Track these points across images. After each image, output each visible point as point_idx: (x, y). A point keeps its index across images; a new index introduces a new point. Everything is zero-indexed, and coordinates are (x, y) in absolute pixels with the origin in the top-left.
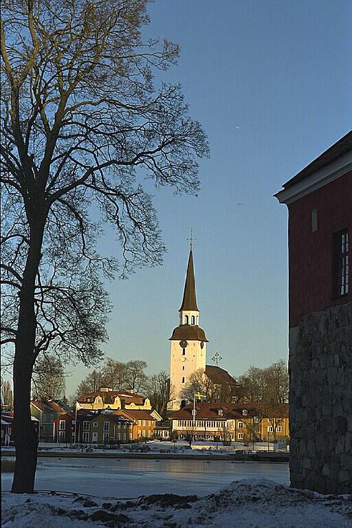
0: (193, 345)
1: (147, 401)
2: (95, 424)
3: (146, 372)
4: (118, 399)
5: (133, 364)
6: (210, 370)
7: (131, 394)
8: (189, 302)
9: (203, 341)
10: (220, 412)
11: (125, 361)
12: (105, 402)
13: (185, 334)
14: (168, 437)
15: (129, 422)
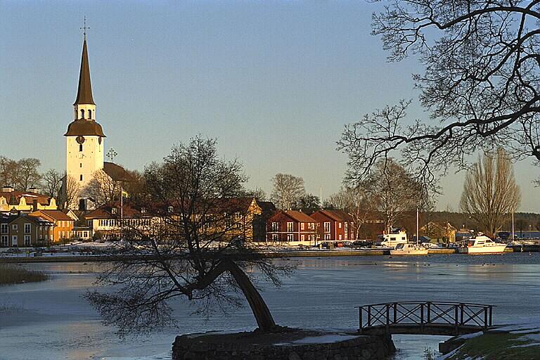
0: (91, 140)
1: (53, 201)
2: (15, 227)
3: (40, 170)
4: (23, 199)
5: (24, 162)
6: (109, 168)
7: (35, 194)
8: (84, 95)
9: (101, 136)
12: (10, 203)
13: (82, 129)
14: (88, 238)
15: (50, 223)
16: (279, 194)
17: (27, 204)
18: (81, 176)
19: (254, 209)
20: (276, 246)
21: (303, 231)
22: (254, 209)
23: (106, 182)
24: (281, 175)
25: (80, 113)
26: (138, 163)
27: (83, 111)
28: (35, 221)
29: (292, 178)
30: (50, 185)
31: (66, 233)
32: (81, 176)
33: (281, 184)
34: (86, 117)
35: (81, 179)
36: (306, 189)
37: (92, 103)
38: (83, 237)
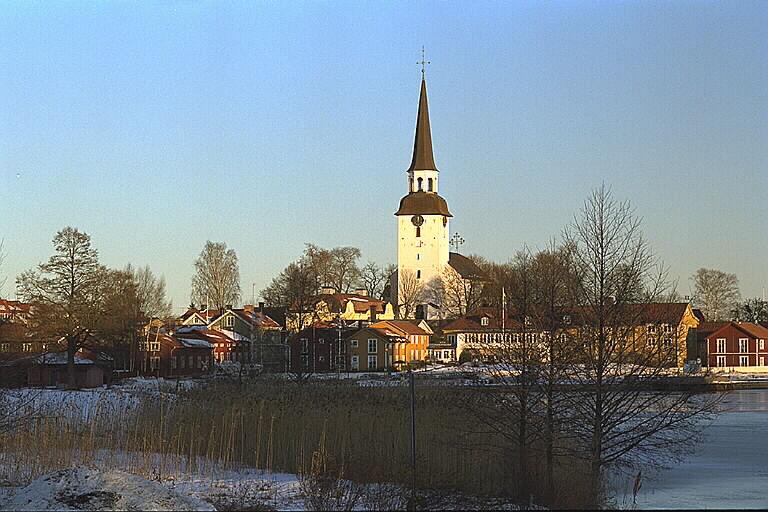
0: (432, 222)
3: (360, 264)
4: (350, 305)
5: (337, 252)
8: (422, 157)
10: (484, 321)
11: (329, 249)
13: (419, 205)
16: (702, 297)
17: (356, 312)
18: (419, 272)
19: (690, 321)
20: (745, 371)
21: (762, 351)
22: (690, 321)
23: (449, 276)
24: (703, 271)
25: (416, 183)
26: (500, 251)
27: (420, 180)
28: (376, 332)
29: (721, 275)
30: (368, 285)
31: (420, 353)
32: (419, 272)
33: (704, 284)
34: (425, 188)
35: (419, 277)
36: (741, 292)
37: (434, 169)
38: (443, 358)
